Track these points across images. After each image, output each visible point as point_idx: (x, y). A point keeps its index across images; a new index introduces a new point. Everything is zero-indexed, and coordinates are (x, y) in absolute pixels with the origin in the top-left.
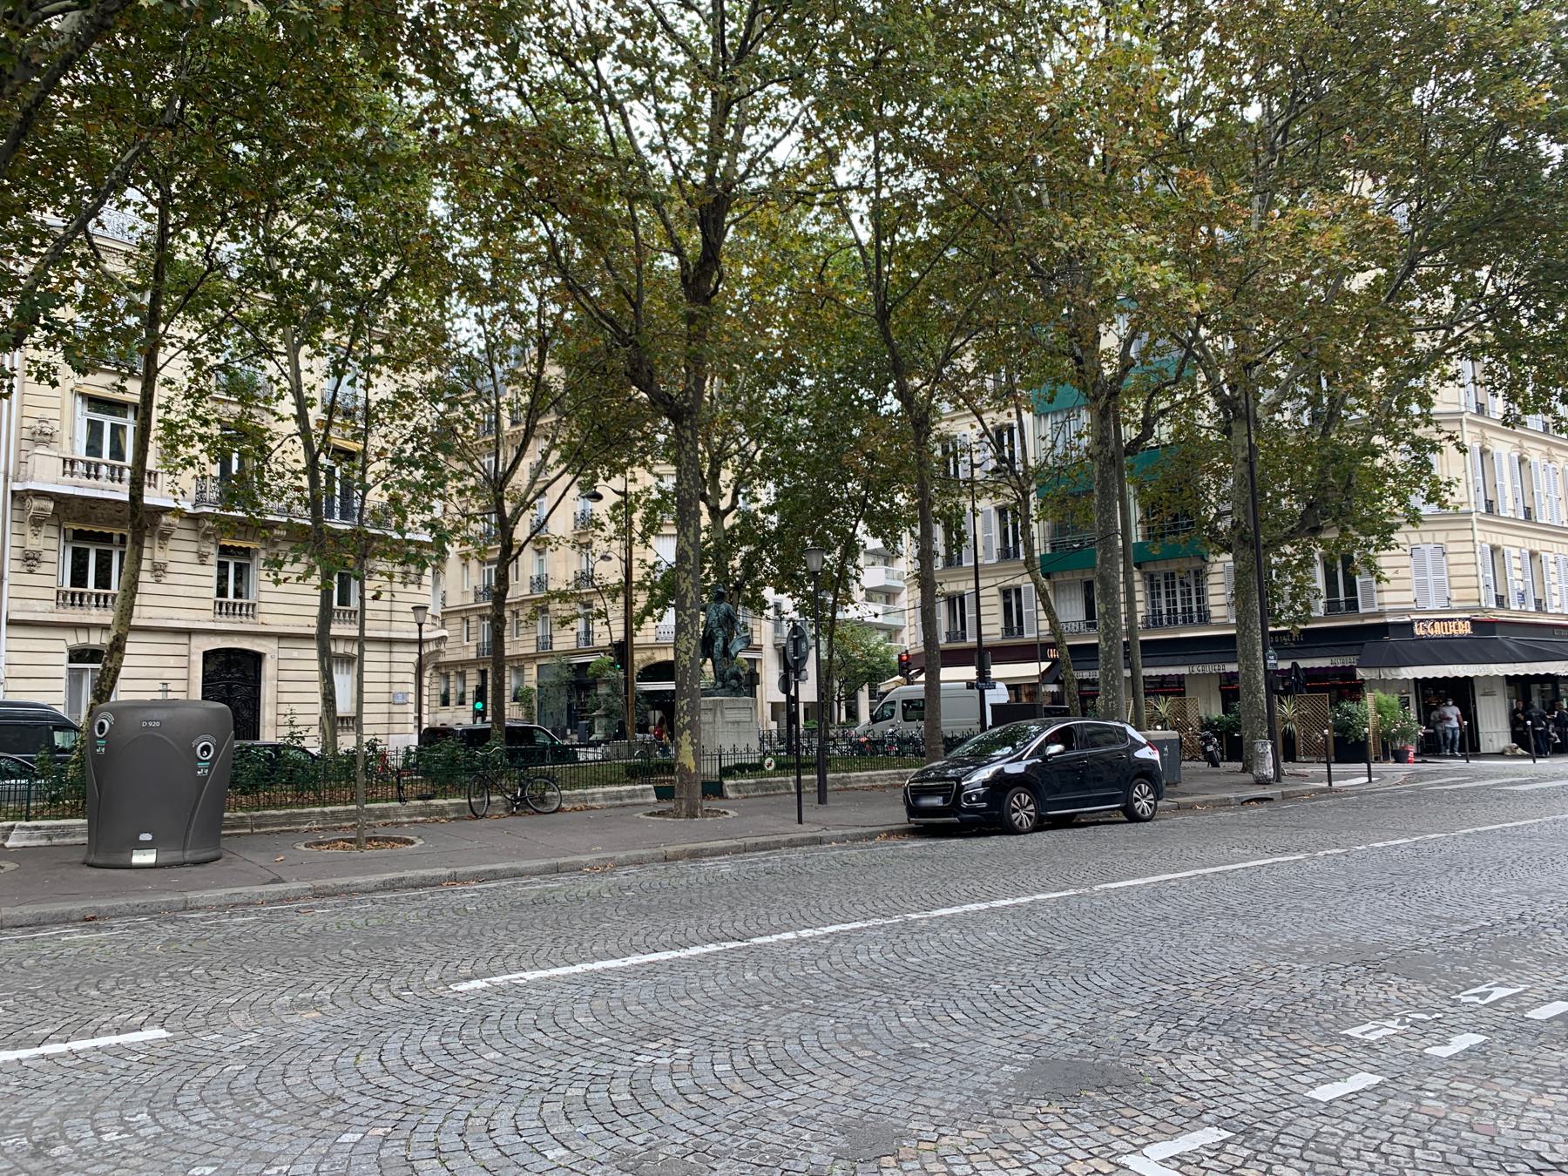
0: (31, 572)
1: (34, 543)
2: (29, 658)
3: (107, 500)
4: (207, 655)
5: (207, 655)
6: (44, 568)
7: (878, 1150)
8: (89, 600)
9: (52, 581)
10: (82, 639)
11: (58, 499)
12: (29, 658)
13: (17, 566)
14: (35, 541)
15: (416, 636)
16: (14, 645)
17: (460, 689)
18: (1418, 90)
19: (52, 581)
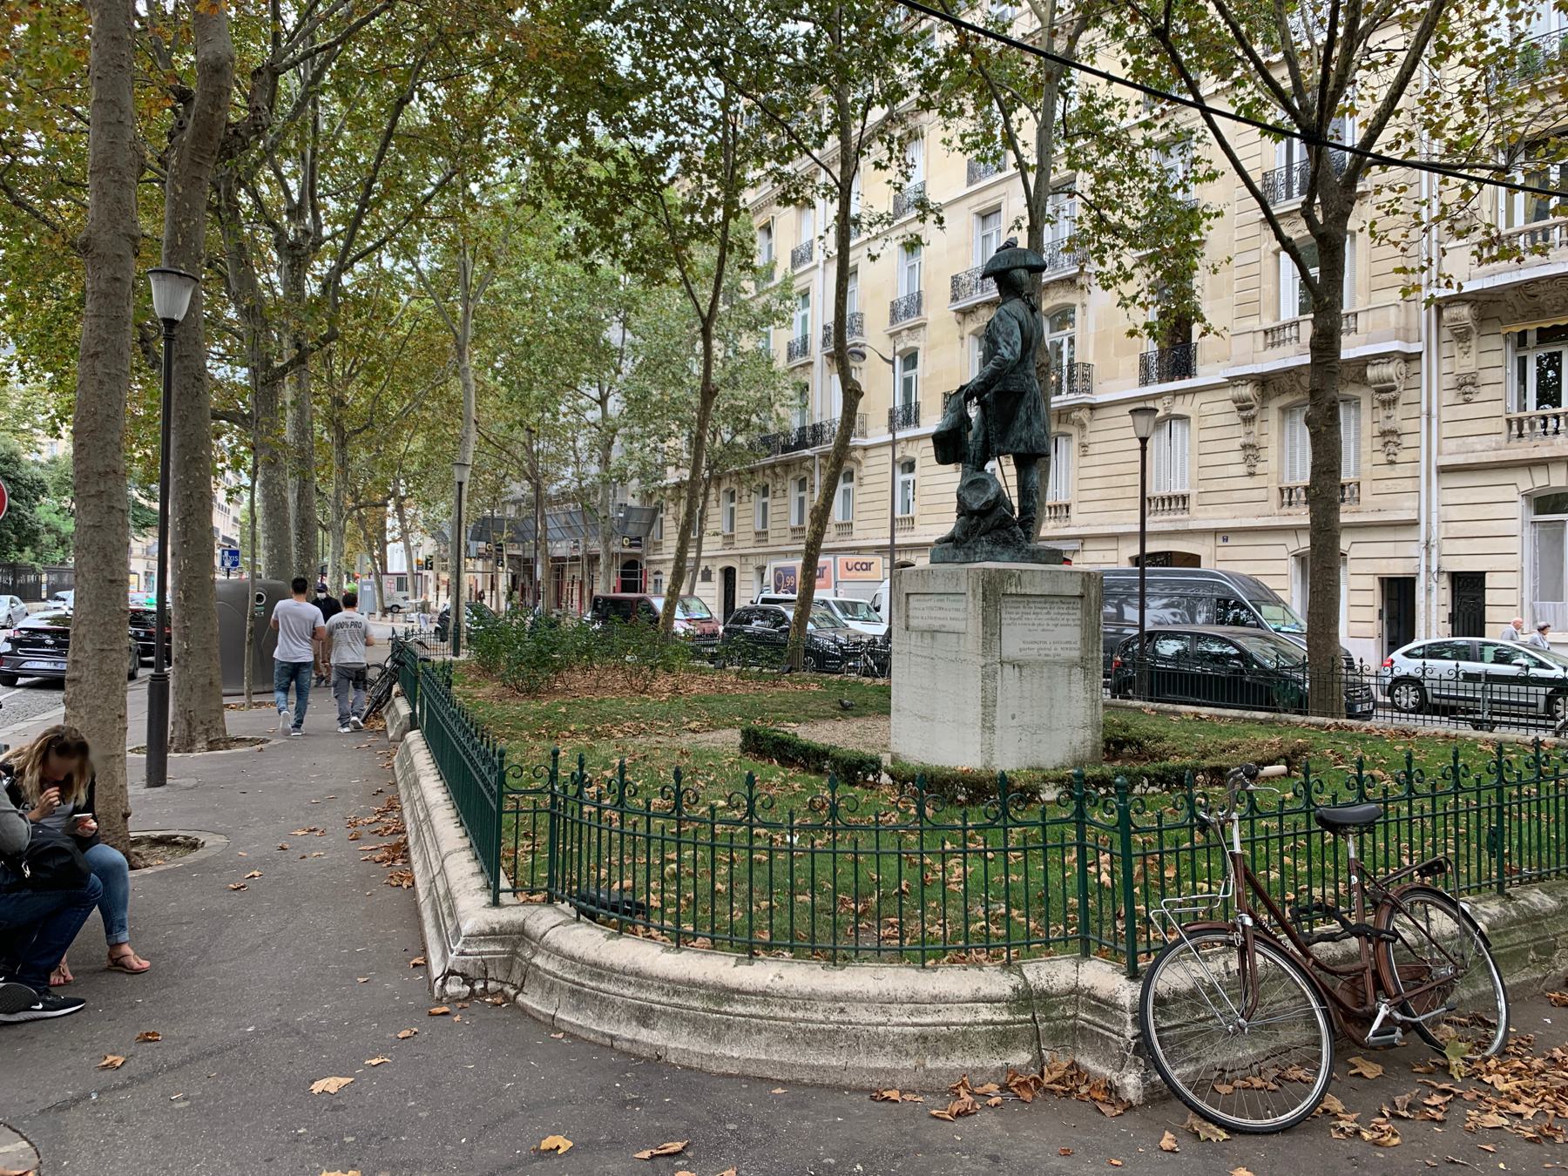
0: (1467, 401)
1: (1467, 363)
2: (1467, 513)
3: (1535, 281)
4: (776, 570)
5: (776, 570)
6: (1486, 393)
7: (1167, 1156)
8: (1532, 425)
9: (1498, 408)
10: (1541, 480)
11: (1474, 300)
12: (1467, 513)
13: (1449, 397)
14: (1465, 361)
15: (888, 542)
16: (1451, 497)
17: (940, 580)
18: (29, 892)
19: (1498, 408)
